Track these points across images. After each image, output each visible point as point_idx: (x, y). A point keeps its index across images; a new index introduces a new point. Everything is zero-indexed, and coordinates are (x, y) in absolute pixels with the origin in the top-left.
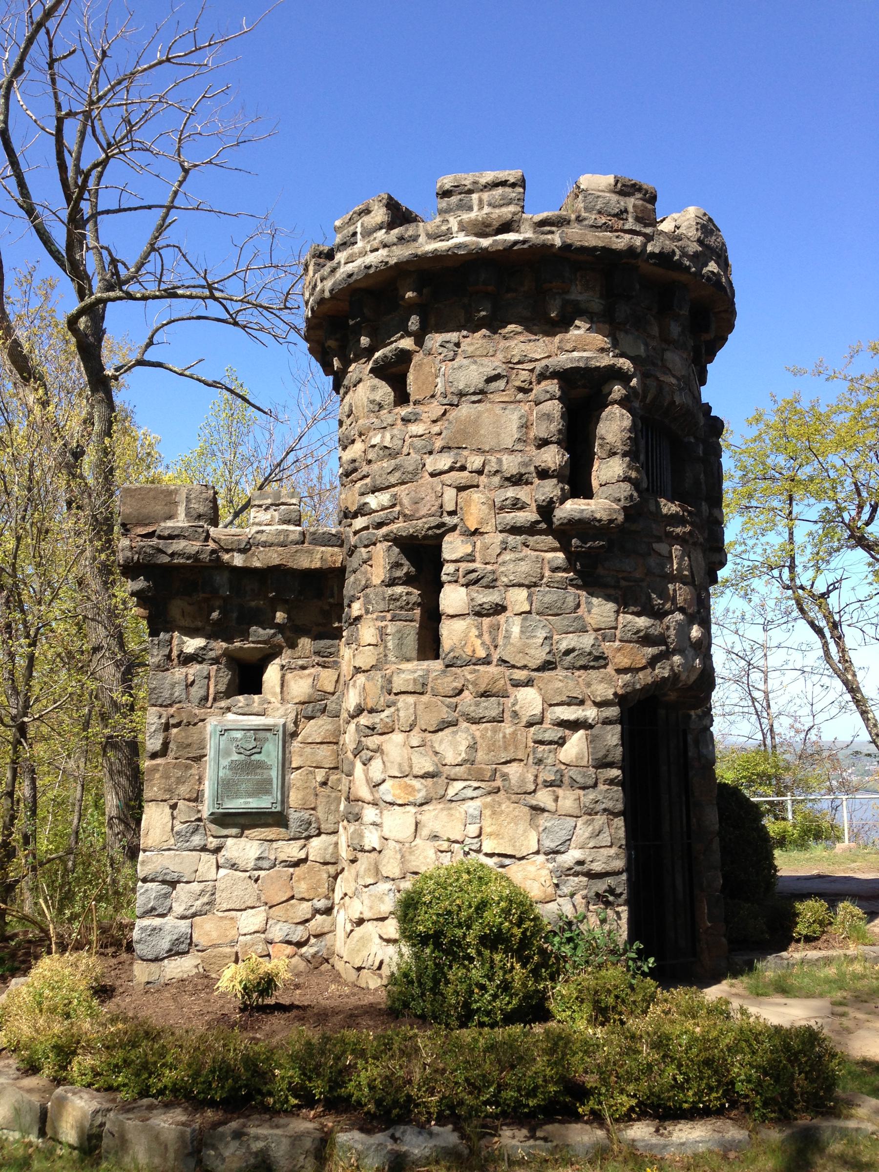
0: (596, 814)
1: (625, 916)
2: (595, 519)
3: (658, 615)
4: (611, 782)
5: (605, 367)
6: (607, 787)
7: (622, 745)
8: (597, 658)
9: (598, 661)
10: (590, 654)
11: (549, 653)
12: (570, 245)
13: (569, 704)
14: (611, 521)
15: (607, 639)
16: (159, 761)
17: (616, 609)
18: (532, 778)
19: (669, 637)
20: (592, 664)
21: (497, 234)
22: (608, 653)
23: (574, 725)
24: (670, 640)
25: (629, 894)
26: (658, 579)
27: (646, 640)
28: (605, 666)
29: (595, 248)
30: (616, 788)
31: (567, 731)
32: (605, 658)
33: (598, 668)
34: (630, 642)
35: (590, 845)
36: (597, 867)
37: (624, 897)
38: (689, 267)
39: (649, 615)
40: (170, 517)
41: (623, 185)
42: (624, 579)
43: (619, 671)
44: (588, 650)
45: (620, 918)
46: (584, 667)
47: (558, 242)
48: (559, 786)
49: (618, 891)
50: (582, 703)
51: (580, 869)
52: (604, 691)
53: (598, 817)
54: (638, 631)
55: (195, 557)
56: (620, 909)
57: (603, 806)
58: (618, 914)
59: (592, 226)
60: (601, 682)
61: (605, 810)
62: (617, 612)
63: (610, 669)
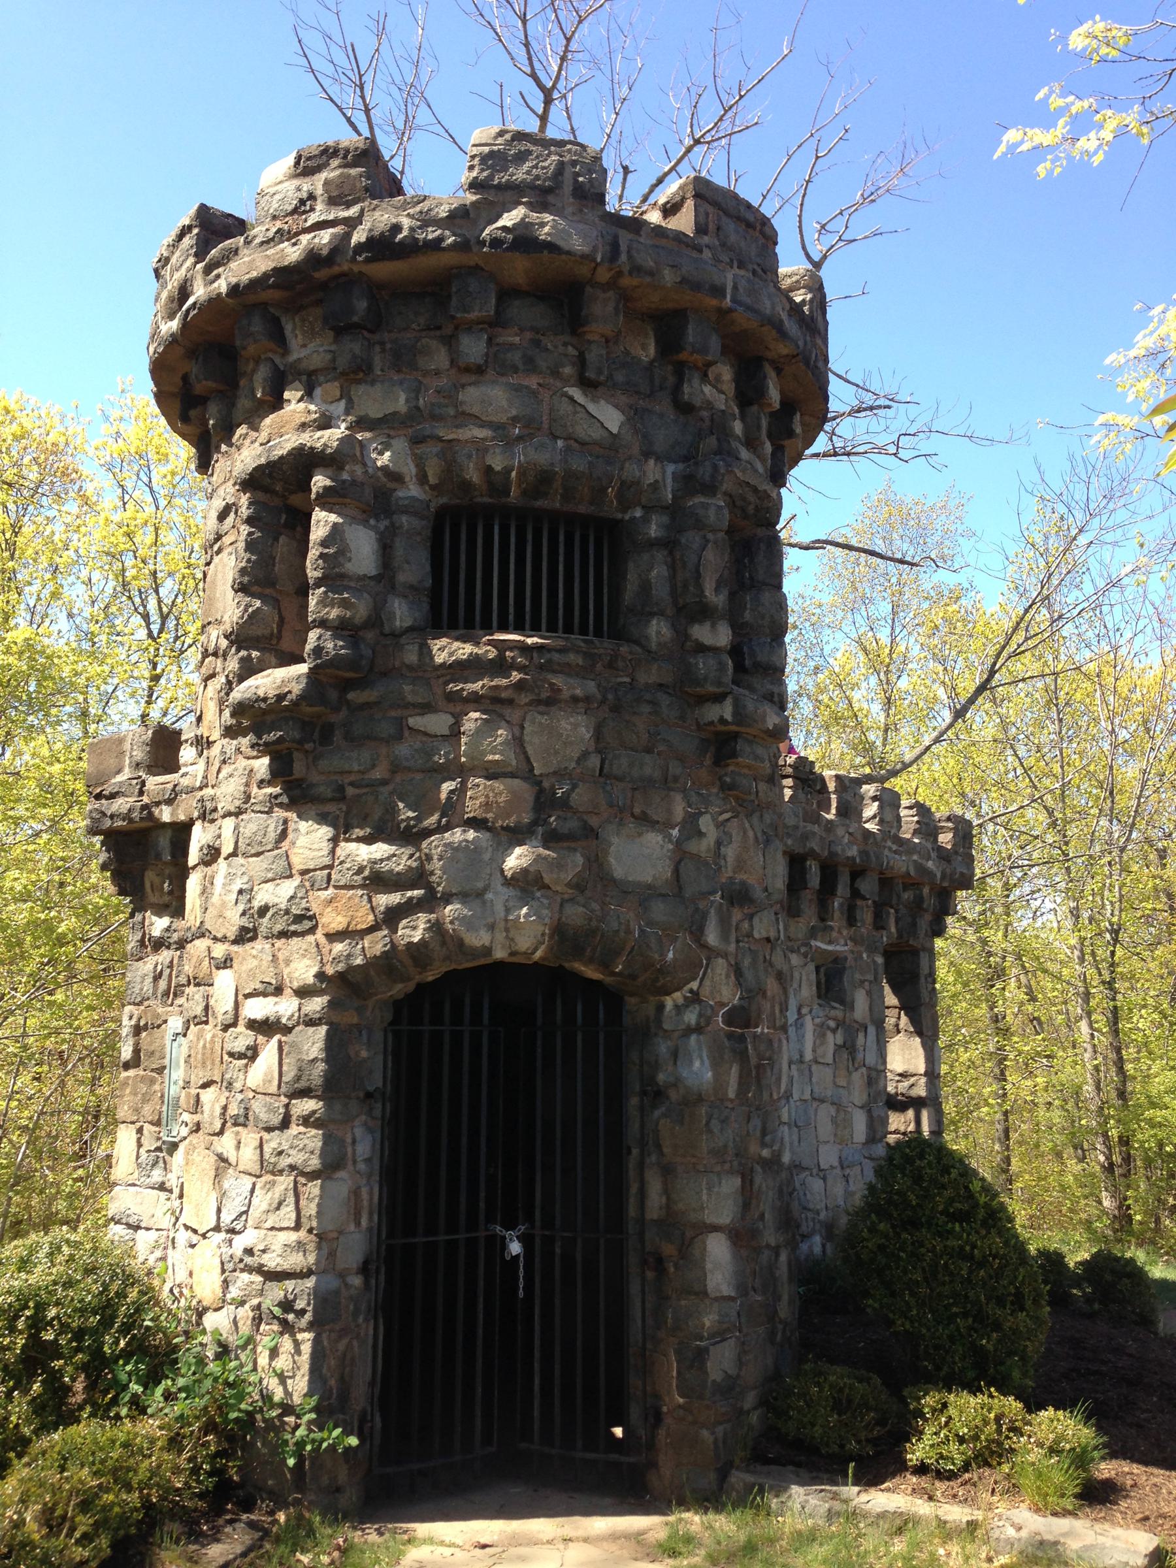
0: (281, 1172)
1: (306, 1348)
2: (258, 699)
3: (410, 836)
4: (306, 1121)
5: (290, 453)
6: (302, 1129)
7: (327, 1061)
8: (299, 919)
9: (301, 922)
10: (287, 912)
11: (244, 914)
12: (237, 286)
13: (265, 994)
14: (280, 697)
15: (316, 886)
16: (131, 1073)
17: (330, 835)
18: (218, 1111)
19: (432, 873)
20: (293, 928)
21: (181, 306)
22: (315, 909)
23: (265, 1027)
24: (433, 878)
25: (315, 1311)
26: (418, 776)
27: (377, 880)
28: (312, 930)
29: (266, 276)
30: (314, 1132)
31: (260, 1037)
32: (312, 917)
33: (302, 934)
34: (352, 887)
35: (268, 1225)
36: (272, 1261)
37: (308, 1316)
38: (440, 239)
39: (388, 840)
40: (119, 772)
41: (309, 159)
42: (352, 784)
43: (332, 937)
44: (283, 906)
45: (298, 1351)
46: (284, 934)
47: (224, 289)
48: (245, 1125)
49: (300, 1304)
50: (278, 991)
51: (249, 1262)
52: (304, 970)
53: (281, 1178)
54: (361, 870)
55: (127, 817)
56: (299, 1336)
57: (289, 1161)
58: (297, 1344)
59: (263, 243)
60: (304, 956)
61: (292, 1168)
62: (335, 841)
63: (319, 935)
